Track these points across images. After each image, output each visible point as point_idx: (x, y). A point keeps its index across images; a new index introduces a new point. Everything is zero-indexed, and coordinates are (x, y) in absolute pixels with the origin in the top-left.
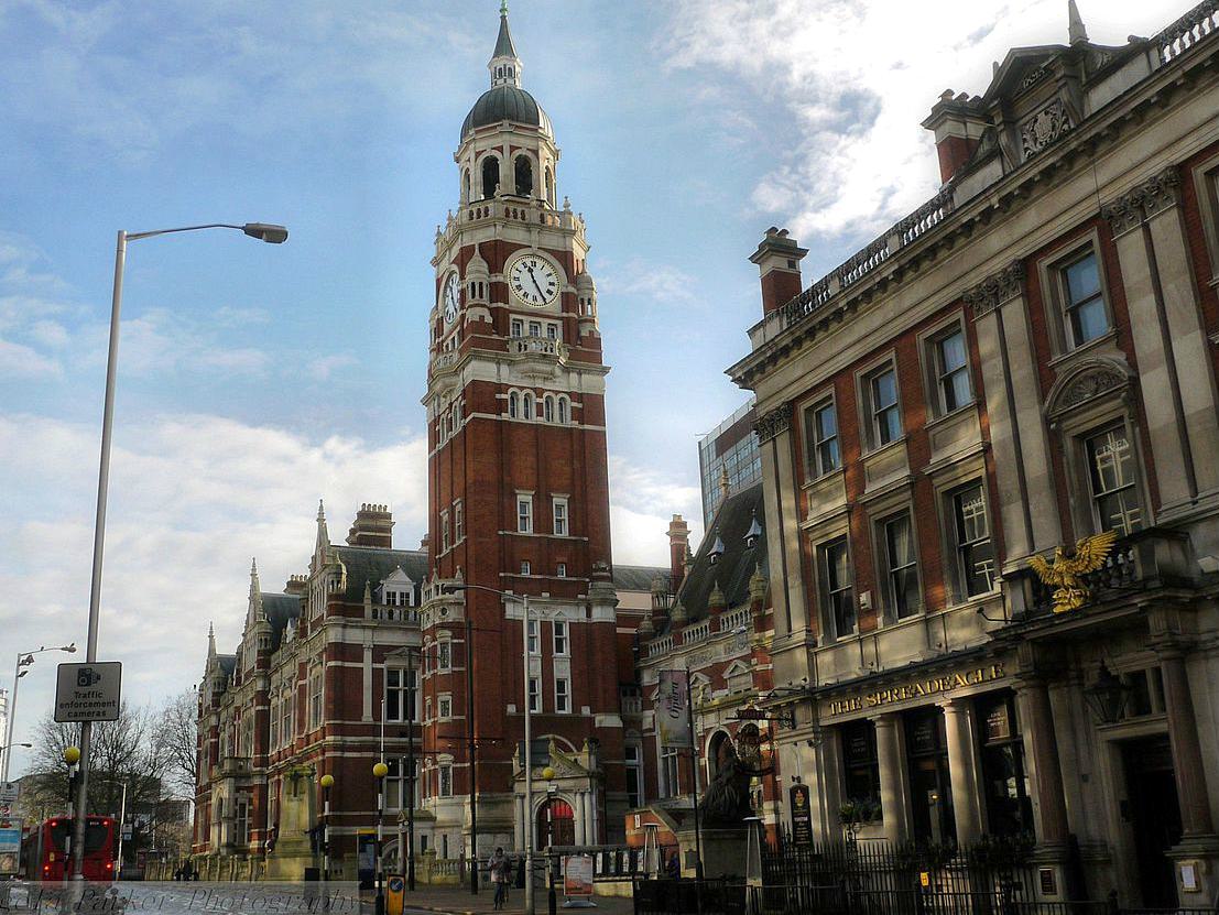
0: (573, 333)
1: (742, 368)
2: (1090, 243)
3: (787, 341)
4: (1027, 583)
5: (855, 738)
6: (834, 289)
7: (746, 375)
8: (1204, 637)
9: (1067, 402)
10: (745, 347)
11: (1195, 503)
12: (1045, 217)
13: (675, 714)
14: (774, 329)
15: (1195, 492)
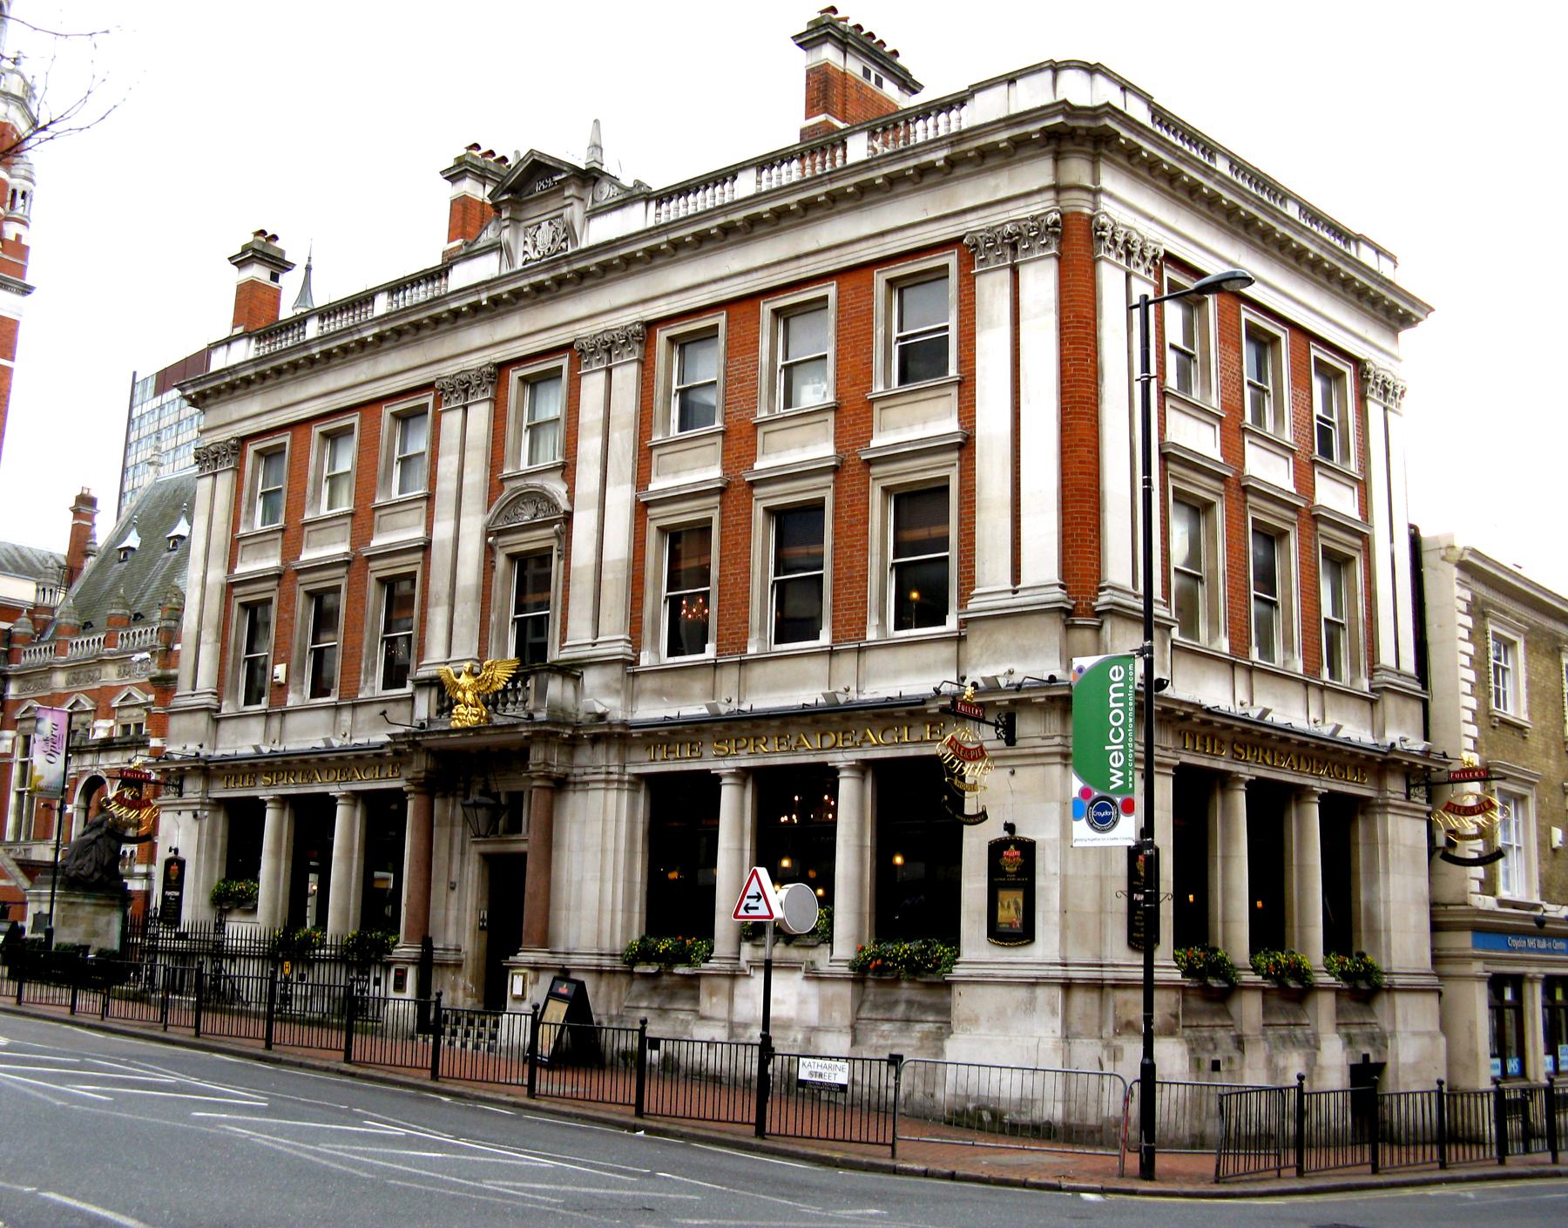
4: (434, 692)
8: (576, 771)
11: (1015, 592)
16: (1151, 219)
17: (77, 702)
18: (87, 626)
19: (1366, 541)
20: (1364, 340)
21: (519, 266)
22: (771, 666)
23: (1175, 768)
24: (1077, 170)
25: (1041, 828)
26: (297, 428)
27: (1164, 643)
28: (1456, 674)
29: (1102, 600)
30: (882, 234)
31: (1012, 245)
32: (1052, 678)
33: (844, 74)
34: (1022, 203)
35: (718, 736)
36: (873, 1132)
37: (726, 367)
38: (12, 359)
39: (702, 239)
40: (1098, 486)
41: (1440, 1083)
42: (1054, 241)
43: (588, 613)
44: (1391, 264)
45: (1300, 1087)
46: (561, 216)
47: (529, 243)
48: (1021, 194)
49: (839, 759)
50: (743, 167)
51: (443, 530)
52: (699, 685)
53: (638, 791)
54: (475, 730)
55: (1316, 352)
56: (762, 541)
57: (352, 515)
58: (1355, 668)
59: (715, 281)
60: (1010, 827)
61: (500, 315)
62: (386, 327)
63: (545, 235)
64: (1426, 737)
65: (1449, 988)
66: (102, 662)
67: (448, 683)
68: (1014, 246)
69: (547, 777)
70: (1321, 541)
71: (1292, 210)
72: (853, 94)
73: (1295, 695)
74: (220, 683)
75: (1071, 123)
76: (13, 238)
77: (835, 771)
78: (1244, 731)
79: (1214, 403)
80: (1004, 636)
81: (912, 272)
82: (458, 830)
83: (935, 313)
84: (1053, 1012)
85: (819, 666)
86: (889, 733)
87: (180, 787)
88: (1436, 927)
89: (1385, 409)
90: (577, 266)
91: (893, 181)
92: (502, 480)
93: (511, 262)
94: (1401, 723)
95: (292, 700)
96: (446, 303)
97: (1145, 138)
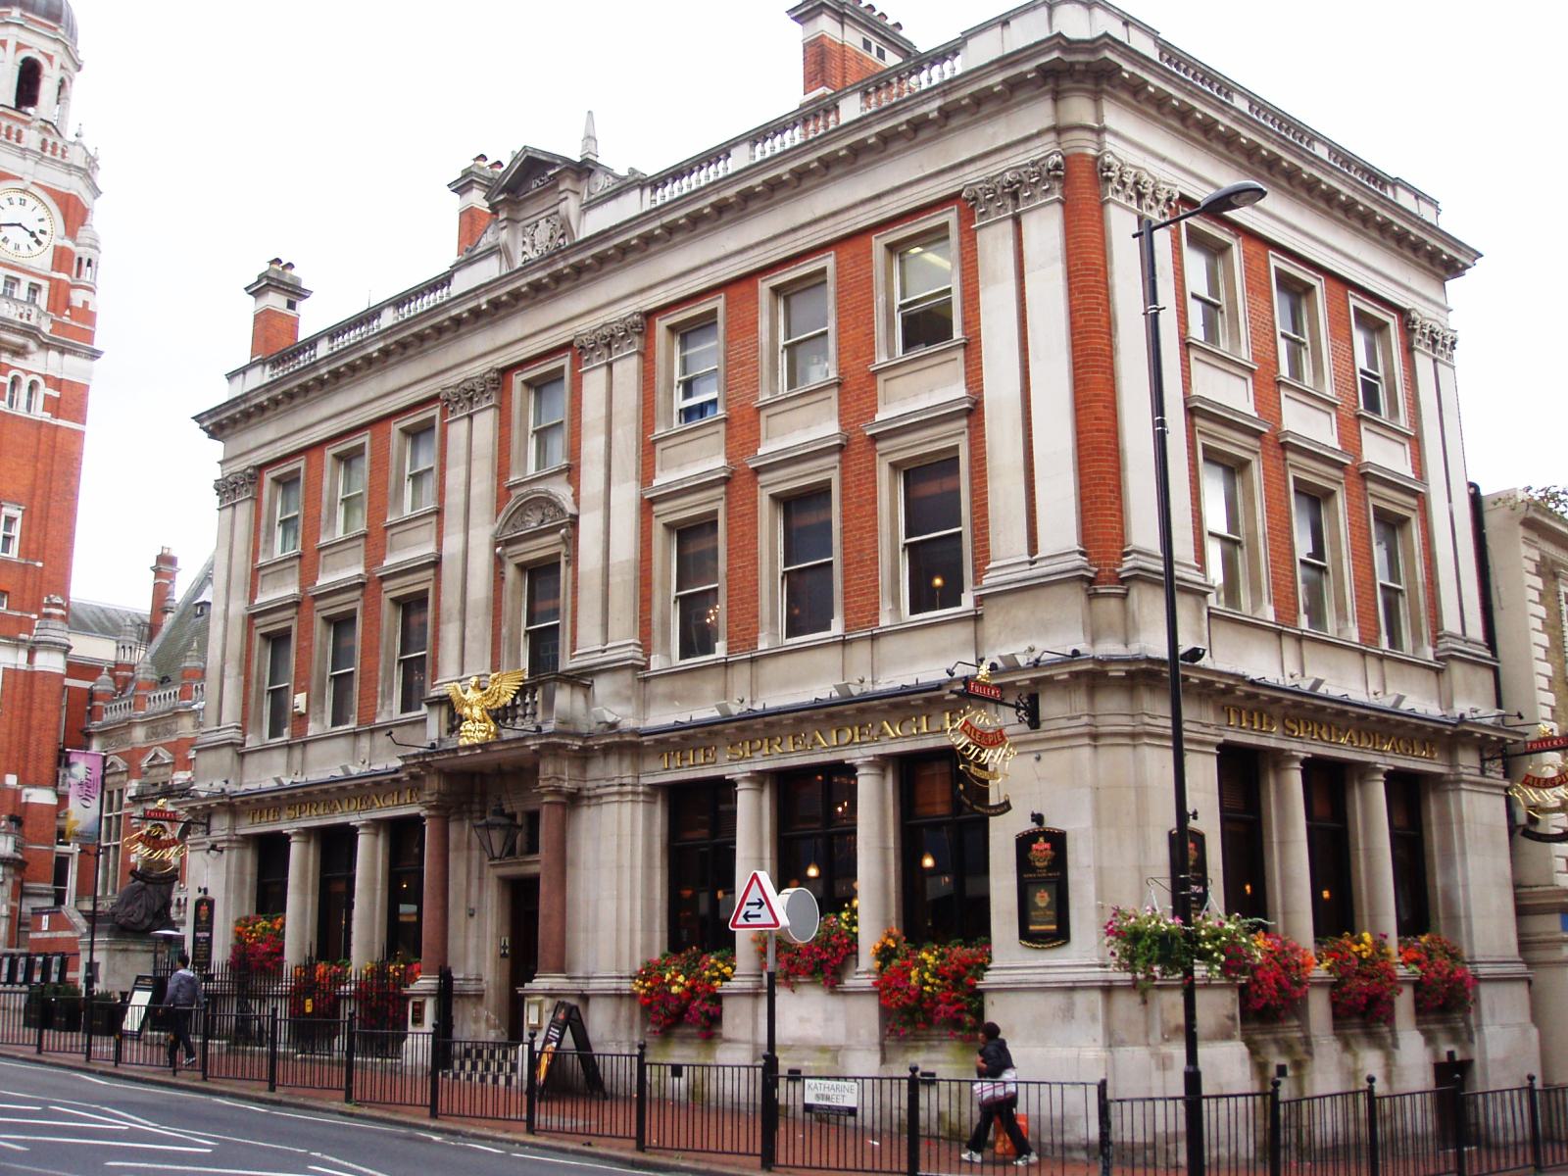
0: (61, 300)
1: (210, 417)
2: (823, 271)
4: (444, 710)
5: (270, 852)
6: (323, 349)
8: (590, 785)
10: (221, 393)
11: (1032, 563)
13: (87, 804)
14: (260, 377)
15: (1033, 547)
16: (1164, 159)
17: (156, 756)
18: (165, 681)
19: (1422, 499)
20: (1408, 289)
22: (783, 661)
23: (1219, 747)
24: (1079, 109)
25: (1073, 819)
26: (311, 453)
27: (1200, 610)
28: (1528, 638)
29: (1126, 566)
30: (878, 197)
31: (1013, 193)
32: (1076, 653)
33: (843, 46)
34: (1021, 148)
35: (732, 739)
37: (727, 352)
38: (84, 423)
39: (696, 221)
40: (1117, 444)
41: (1531, 1078)
42: (1057, 185)
43: (597, 618)
44: (1433, 211)
45: (1370, 1092)
46: (557, 213)
47: (526, 244)
48: (1020, 136)
49: (856, 755)
50: (735, 142)
51: (452, 544)
52: (710, 686)
53: (655, 803)
54: (484, 746)
55: (1354, 301)
56: (770, 531)
57: (365, 536)
58: (1417, 636)
59: (711, 263)
60: (1038, 818)
61: (502, 318)
62: (390, 341)
63: (543, 233)
64: (1499, 704)
65: (1541, 976)
66: (178, 715)
67: (455, 699)
68: (1015, 196)
69: (558, 791)
70: (1372, 501)
71: (1321, 151)
72: (852, 65)
73: (1351, 664)
74: (244, 719)
75: (1069, 58)
76: (80, 305)
78: (1296, 705)
79: (1245, 355)
80: (1021, 611)
81: (908, 230)
82: (476, 853)
83: (935, 269)
84: (1094, 1018)
85: (833, 657)
86: (907, 724)
87: (208, 825)
88: (1522, 911)
89: (1435, 361)
90: (572, 260)
91: (886, 139)
92: (509, 488)
93: (510, 260)
94: (1470, 694)
95: (313, 729)
96: (447, 310)
97: (1151, 71)
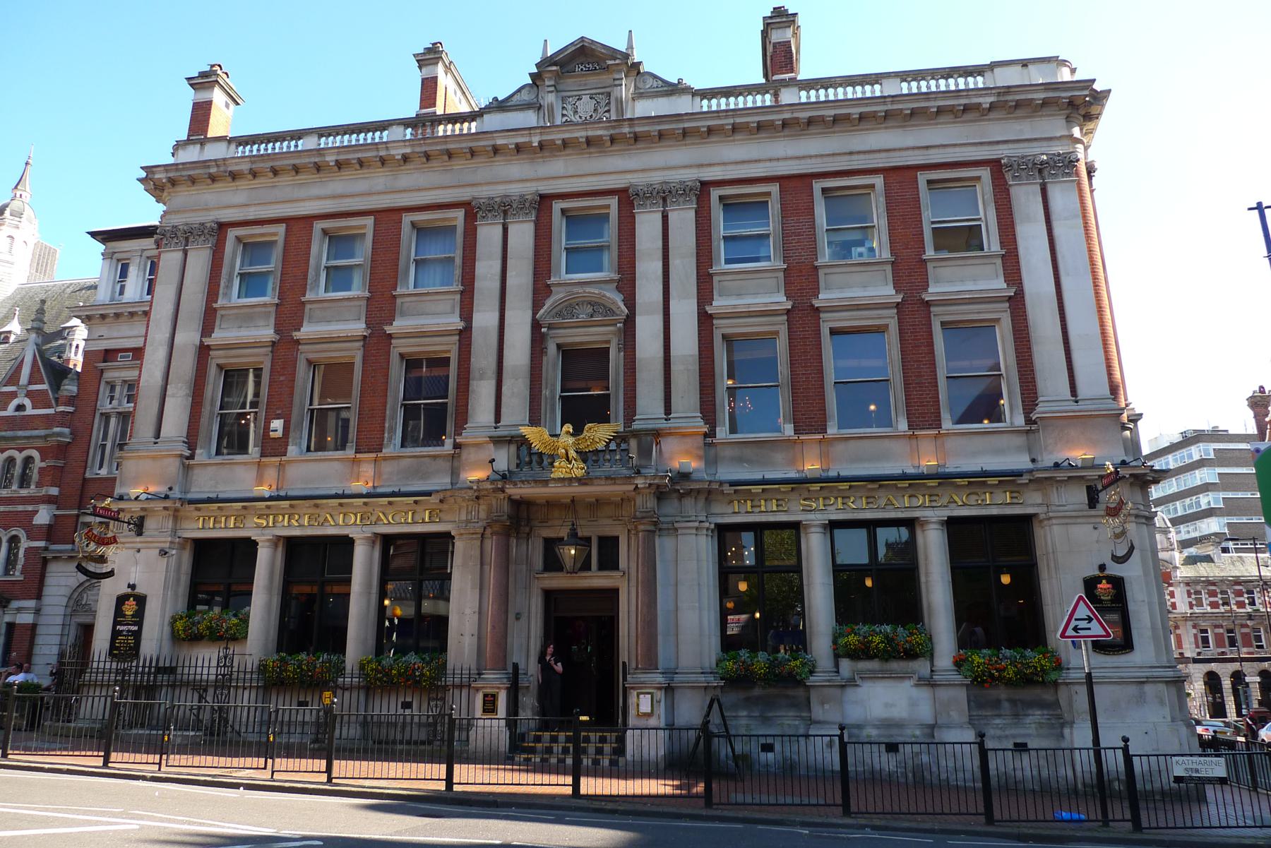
3: (245, 167)
4: (513, 448)
7: (158, 182)
9: (559, 314)
12: (571, 171)
15: (498, 418)
21: (558, 122)
36: (913, 805)
77: (255, 543)
